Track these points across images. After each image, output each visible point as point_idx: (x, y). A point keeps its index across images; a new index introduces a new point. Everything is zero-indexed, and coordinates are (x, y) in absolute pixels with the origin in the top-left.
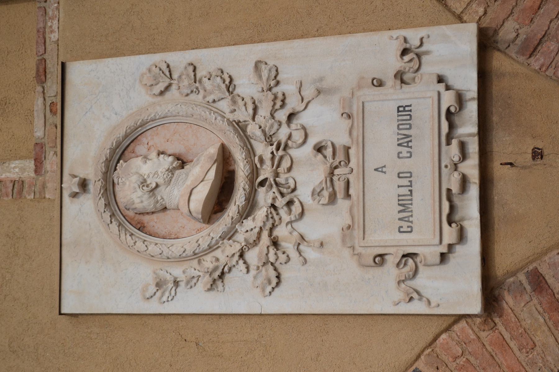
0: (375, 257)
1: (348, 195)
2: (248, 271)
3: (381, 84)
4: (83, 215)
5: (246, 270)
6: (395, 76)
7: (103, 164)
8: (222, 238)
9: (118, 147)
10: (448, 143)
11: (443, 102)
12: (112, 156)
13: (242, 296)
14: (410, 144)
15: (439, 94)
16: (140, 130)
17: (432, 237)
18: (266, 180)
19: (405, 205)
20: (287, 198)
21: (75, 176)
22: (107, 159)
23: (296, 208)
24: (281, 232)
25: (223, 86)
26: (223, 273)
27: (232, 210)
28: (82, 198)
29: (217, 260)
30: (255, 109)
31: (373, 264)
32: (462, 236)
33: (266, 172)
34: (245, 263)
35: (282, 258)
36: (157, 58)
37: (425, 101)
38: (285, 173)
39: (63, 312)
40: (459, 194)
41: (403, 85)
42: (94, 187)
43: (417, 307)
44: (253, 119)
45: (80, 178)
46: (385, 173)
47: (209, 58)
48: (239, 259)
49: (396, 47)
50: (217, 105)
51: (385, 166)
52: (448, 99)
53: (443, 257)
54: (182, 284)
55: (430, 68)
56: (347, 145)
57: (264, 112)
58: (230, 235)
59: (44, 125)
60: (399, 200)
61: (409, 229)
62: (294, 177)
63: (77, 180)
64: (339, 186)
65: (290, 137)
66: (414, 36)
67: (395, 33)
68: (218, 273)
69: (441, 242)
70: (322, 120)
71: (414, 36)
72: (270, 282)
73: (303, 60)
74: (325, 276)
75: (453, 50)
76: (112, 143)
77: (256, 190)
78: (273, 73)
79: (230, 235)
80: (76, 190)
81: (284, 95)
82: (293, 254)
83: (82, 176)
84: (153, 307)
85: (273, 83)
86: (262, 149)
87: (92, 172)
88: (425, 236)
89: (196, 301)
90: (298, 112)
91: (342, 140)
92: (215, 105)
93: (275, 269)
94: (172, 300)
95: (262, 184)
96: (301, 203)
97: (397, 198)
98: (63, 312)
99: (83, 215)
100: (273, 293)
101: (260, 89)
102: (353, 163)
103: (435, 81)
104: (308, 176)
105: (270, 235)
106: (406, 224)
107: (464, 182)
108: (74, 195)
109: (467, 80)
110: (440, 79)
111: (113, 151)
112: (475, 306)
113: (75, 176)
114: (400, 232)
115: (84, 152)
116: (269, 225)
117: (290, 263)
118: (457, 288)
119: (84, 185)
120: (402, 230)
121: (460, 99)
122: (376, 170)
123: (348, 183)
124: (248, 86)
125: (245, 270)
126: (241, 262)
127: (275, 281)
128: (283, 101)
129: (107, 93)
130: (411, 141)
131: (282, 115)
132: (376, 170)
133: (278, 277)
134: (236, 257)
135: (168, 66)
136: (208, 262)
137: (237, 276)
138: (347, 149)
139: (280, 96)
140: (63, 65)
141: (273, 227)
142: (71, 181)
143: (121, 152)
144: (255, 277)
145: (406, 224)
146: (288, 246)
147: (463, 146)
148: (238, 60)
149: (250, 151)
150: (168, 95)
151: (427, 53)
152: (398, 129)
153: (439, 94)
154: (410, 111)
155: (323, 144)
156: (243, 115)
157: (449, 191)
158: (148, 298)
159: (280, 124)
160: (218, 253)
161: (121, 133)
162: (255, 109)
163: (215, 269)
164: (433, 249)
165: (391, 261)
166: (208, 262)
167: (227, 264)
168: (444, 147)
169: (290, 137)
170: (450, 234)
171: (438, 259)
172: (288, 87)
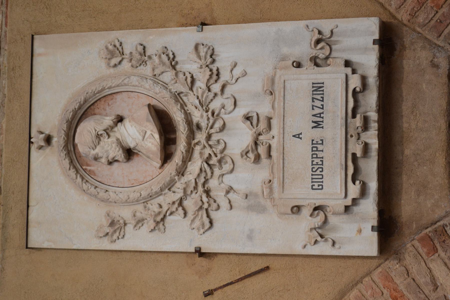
0: (293, 208)
1: (270, 156)
3: (299, 65)
4: (48, 166)
9: (80, 108)
10: (354, 116)
11: (350, 82)
12: (73, 117)
13: (180, 236)
14: (322, 115)
15: (347, 76)
16: (99, 96)
18: (199, 142)
19: (317, 168)
20: (219, 156)
21: (42, 133)
24: (213, 183)
25: (168, 63)
26: (165, 216)
27: (177, 159)
29: (161, 206)
31: (290, 212)
32: (364, 192)
34: (184, 209)
35: (214, 206)
39: (29, 246)
40: (362, 157)
42: (58, 140)
44: (191, 89)
45: (46, 134)
46: (301, 138)
48: (179, 207)
49: (310, 37)
50: (161, 78)
51: (301, 134)
53: (347, 208)
55: (340, 55)
56: (270, 116)
57: (200, 84)
60: (312, 179)
61: (320, 187)
63: (42, 136)
64: (262, 150)
66: (326, 25)
68: (161, 216)
70: (249, 95)
71: (326, 25)
72: (203, 225)
75: (359, 38)
77: (193, 149)
78: (209, 53)
80: (43, 143)
83: (47, 132)
84: (106, 244)
85: (209, 60)
88: (334, 190)
91: (264, 109)
93: (208, 216)
94: (122, 238)
97: (311, 177)
98: (29, 246)
99: (48, 166)
101: (199, 66)
102: (275, 131)
106: (317, 183)
107: (366, 148)
108: (40, 148)
110: (347, 64)
111: (75, 112)
113: (42, 133)
114: (313, 189)
115: (49, 114)
116: (202, 180)
117: (219, 211)
119: (48, 140)
120: (314, 187)
122: (294, 136)
123: (270, 147)
124: (190, 65)
126: (180, 209)
127: (207, 225)
128: (218, 75)
129: (66, 68)
130: (323, 113)
131: (216, 88)
132: (294, 136)
134: (176, 205)
136: (153, 207)
137: (175, 220)
138: (269, 119)
140: (33, 36)
141: (206, 181)
143: (83, 112)
144: (193, 221)
145: (317, 183)
146: (218, 194)
147: (366, 120)
148: (182, 40)
150: (120, 68)
151: (336, 42)
152: (322, 185)
154: (323, 91)
155: (250, 115)
156: (180, 87)
157: (354, 155)
158: (101, 237)
160: (160, 199)
163: (159, 213)
164: (340, 202)
165: (306, 212)
166: (153, 207)
167: (168, 209)
168: (350, 120)
170: (354, 190)
171: (343, 209)
172: (223, 63)
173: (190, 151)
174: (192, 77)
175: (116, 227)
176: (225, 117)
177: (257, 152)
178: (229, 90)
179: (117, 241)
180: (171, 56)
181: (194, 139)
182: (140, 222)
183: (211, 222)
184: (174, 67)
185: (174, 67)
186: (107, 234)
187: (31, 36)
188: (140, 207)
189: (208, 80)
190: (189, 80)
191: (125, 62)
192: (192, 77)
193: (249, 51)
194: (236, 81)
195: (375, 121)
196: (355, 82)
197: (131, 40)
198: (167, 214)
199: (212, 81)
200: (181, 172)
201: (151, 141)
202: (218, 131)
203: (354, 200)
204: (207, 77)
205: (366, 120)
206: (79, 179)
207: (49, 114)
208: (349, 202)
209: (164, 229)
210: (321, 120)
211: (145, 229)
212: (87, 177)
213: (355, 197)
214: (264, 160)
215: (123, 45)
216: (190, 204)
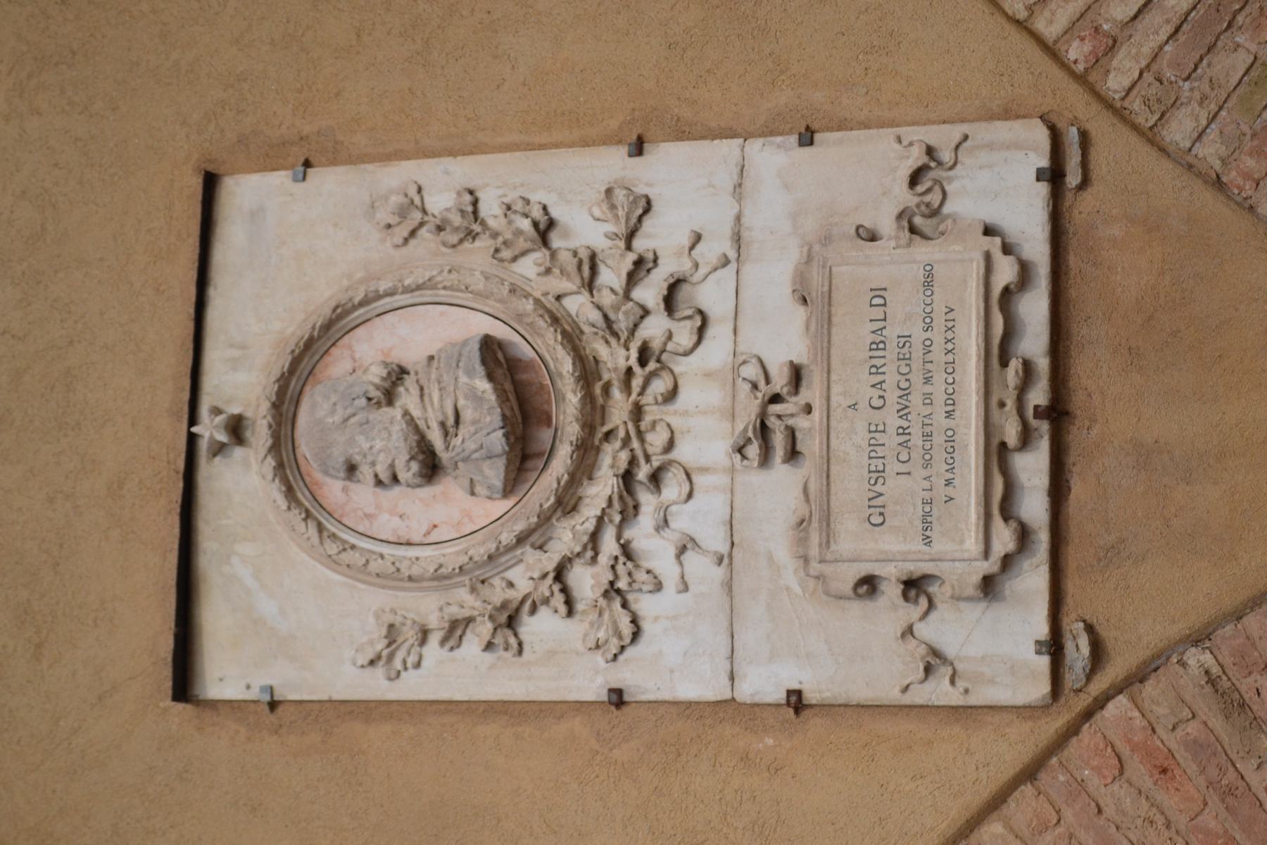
3: (873, 238)
6: (900, 216)
8: (521, 540)
10: (1004, 363)
13: (561, 660)
15: (988, 257)
17: (972, 544)
20: (656, 464)
37: (960, 270)
38: (657, 403)
41: (914, 236)
42: (260, 435)
43: (940, 692)
47: (501, 180)
54: (434, 639)
57: (611, 277)
59: (368, 324)
67: (909, 133)
69: (986, 554)
71: (943, 136)
73: (687, 186)
75: (1002, 187)
80: (222, 437)
81: (655, 253)
83: (235, 410)
84: (375, 686)
86: (614, 358)
88: (961, 548)
100: (621, 658)
103: (981, 229)
104: (701, 420)
105: (619, 537)
118: (1001, 647)
121: (1025, 269)
124: (586, 229)
125: (563, 609)
129: (295, 242)
131: (650, 293)
133: (634, 621)
135: (420, 190)
137: (542, 627)
140: (211, 183)
142: (212, 421)
148: (575, 188)
170: (1004, 539)
173: (586, 453)
175: (394, 648)
177: (766, 439)
179: (403, 674)
181: (603, 424)
182: (456, 630)
184: (545, 242)
187: (197, 183)
188: (463, 594)
193: (745, 226)
195: (641, 483)
196: (1006, 272)
197: (442, 183)
200: (566, 503)
201: (484, 427)
205: (1027, 366)
206: (313, 531)
208: (991, 566)
211: (472, 646)
212: (330, 526)
214: (584, 254)
215: (424, 193)
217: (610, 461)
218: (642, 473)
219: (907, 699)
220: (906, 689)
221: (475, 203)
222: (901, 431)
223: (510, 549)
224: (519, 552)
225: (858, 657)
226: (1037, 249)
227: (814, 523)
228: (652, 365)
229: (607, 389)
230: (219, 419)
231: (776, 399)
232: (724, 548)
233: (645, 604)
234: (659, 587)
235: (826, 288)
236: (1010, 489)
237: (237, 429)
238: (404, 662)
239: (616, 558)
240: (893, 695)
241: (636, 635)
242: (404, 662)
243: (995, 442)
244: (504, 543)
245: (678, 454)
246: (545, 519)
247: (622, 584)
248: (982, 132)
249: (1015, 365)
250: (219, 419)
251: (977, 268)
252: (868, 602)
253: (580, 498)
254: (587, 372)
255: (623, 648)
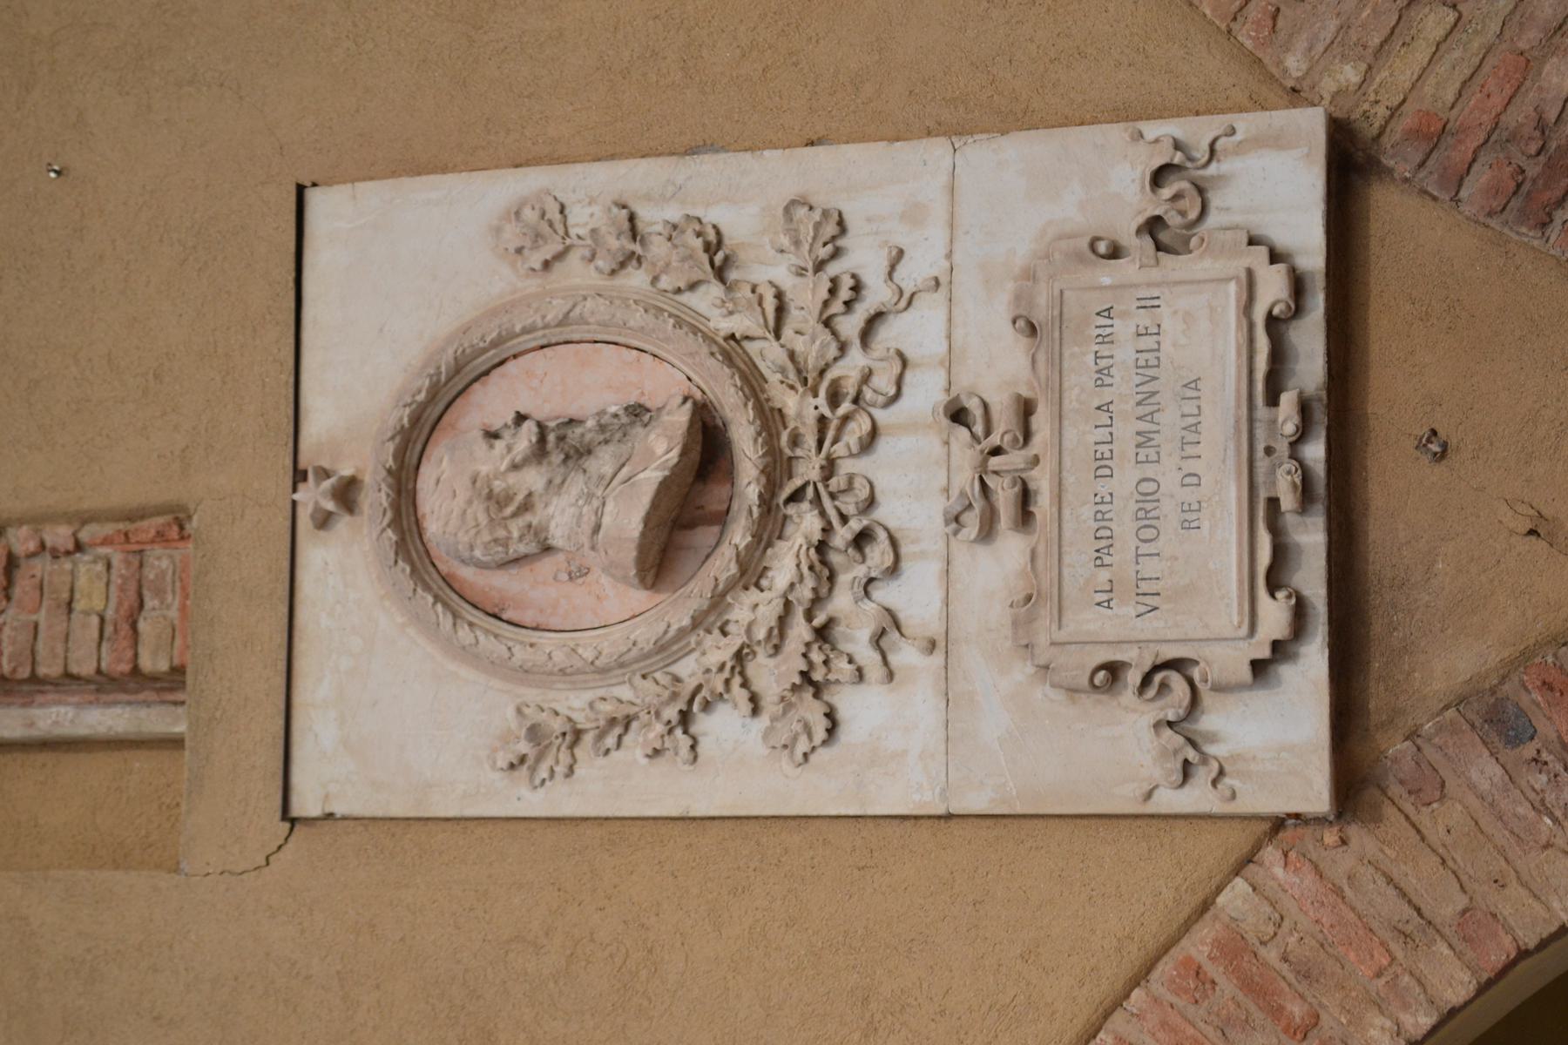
2: (756, 711)
3: (1115, 253)
4: (344, 573)
5: (750, 706)
7: (407, 411)
8: (696, 623)
10: (1273, 400)
13: (740, 765)
20: (856, 525)
22: (389, 471)
23: (878, 554)
28: (344, 523)
30: (781, 310)
33: (808, 470)
36: (534, 179)
38: (851, 455)
41: (1160, 254)
42: (375, 497)
47: (665, 189)
52: (1273, 289)
54: (588, 739)
58: (712, 616)
62: (870, 476)
65: (867, 377)
67: (1152, 130)
70: (954, 340)
71: (1198, 131)
74: (944, 718)
75: (1276, 186)
76: (401, 419)
79: (712, 616)
82: (867, 656)
83: (347, 471)
86: (800, 408)
87: (367, 460)
89: (624, 783)
90: (889, 312)
92: (678, 298)
95: (796, 496)
96: (886, 529)
99: (344, 573)
104: (912, 477)
108: (324, 521)
109: (1308, 239)
112: (1316, 796)
115: (351, 394)
118: (1279, 738)
119: (347, 493)
121: (1298, 286)
124: (770, 267)
125: (746, 707)
127: (820, 734)
129: (401, 268)
131: (850, 326)
137: (724, 727)
139: (847, 282)
140: (300, 190)
146: (857, 640)
148: (742, 194)
149: (770, 419)
153: (1250, 273)
156: (741, 323)
159: (843, 348)
161: (448, 357)
162: (781, 310)
168: (1262, 411)
169: (867, 377)
170: (1274, 616)
171: (1246, 673)
172: (863, 257)
174: (779, 296)
175: (544, 746)
176: (879, 414)
178: (887, 335)
180: (712, 237)
181: (790, 477)
183: (832, 730)
185: (720, 273)
186: (523, 759)
189: (826, 304)
190: (770, 304)
191: (574, 258)
192: (779, 296)
194: (909, 303)
195: (837, 550)
197: (589, 190)
198: (696, 707)
199: (837, 307)
200: (751, 573)
202: (855, 450)
203: (1276, 645)
204: (824, 294)
207: (351, 394)
209: (693, 747)
210: (1155, 428)
213: (1278, 636)
216: (771, 674)
217: (805, 524)
218: (842, 536)
219: (1150, 808)
220: (1149, 795)
221: (632, 218)
222: (1099, 516)
223: (682, 633)
224: (693, 639)
225: (1118, 754)
226: (1313, 259)
227: (1032, 602)
228: (846, 407)
229: (795, 441)
230: (327, 484)
231: (996, 451)
232: (936, 629)
233: (848, 701)
234: (860, 674)
235: (1056, 313)
236: (1281, 552)
237: (347, 493)
238: (552, 771)
239: (808, 645)
240: (1124, 800)
241: (832, 730)
242: (552, 771)
243: (1263, 495)
244: (741, 547)
245: (882, 513)
246: (719, 601)
247: (817, 676)
248: (1246, 124)
249: (1288, 400)
250: (327, 484)
251: (1233, 292)
252: (1104, 697)
253: (766, 568)
254: (770, 419)
255: (814, 749)
